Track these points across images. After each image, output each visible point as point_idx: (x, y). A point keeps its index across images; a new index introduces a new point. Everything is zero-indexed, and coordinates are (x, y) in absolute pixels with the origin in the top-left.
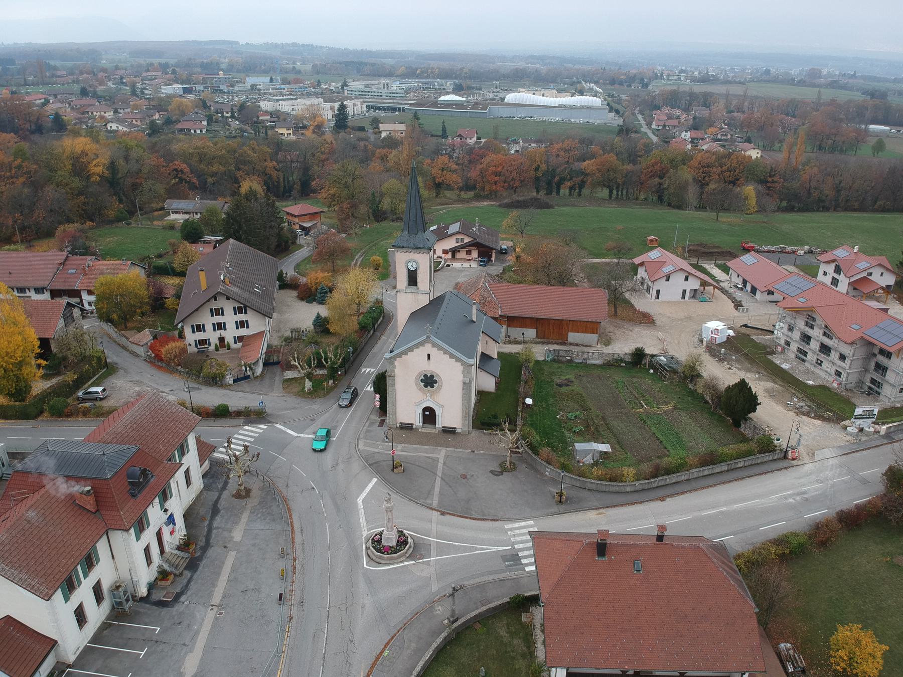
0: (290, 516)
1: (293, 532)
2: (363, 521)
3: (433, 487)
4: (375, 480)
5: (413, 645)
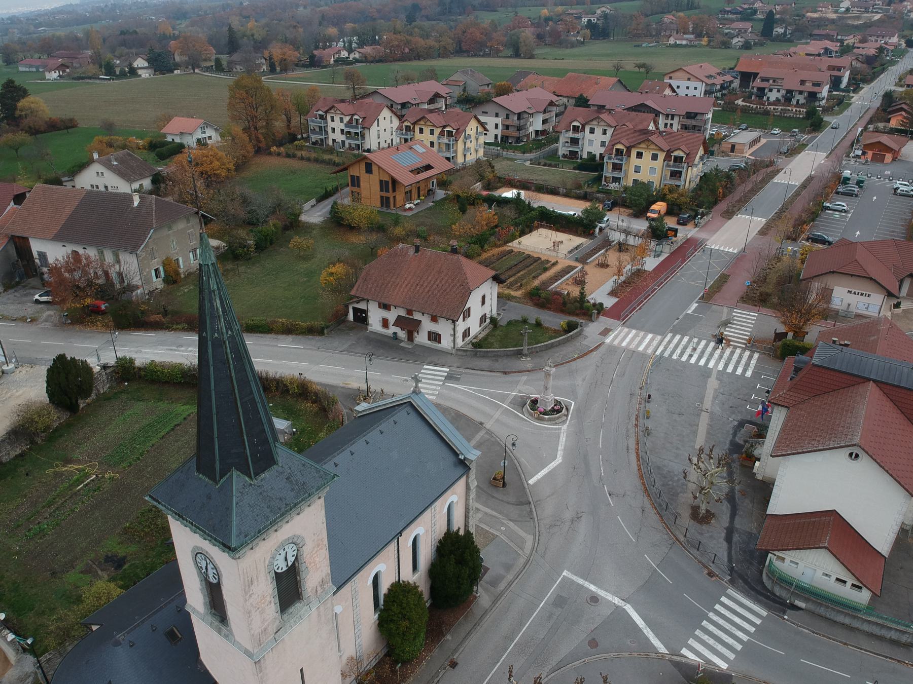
0: (640, 469)
1: (637, 449)
2: (563, 439)
4: (531, 482)
5: (557, 355)
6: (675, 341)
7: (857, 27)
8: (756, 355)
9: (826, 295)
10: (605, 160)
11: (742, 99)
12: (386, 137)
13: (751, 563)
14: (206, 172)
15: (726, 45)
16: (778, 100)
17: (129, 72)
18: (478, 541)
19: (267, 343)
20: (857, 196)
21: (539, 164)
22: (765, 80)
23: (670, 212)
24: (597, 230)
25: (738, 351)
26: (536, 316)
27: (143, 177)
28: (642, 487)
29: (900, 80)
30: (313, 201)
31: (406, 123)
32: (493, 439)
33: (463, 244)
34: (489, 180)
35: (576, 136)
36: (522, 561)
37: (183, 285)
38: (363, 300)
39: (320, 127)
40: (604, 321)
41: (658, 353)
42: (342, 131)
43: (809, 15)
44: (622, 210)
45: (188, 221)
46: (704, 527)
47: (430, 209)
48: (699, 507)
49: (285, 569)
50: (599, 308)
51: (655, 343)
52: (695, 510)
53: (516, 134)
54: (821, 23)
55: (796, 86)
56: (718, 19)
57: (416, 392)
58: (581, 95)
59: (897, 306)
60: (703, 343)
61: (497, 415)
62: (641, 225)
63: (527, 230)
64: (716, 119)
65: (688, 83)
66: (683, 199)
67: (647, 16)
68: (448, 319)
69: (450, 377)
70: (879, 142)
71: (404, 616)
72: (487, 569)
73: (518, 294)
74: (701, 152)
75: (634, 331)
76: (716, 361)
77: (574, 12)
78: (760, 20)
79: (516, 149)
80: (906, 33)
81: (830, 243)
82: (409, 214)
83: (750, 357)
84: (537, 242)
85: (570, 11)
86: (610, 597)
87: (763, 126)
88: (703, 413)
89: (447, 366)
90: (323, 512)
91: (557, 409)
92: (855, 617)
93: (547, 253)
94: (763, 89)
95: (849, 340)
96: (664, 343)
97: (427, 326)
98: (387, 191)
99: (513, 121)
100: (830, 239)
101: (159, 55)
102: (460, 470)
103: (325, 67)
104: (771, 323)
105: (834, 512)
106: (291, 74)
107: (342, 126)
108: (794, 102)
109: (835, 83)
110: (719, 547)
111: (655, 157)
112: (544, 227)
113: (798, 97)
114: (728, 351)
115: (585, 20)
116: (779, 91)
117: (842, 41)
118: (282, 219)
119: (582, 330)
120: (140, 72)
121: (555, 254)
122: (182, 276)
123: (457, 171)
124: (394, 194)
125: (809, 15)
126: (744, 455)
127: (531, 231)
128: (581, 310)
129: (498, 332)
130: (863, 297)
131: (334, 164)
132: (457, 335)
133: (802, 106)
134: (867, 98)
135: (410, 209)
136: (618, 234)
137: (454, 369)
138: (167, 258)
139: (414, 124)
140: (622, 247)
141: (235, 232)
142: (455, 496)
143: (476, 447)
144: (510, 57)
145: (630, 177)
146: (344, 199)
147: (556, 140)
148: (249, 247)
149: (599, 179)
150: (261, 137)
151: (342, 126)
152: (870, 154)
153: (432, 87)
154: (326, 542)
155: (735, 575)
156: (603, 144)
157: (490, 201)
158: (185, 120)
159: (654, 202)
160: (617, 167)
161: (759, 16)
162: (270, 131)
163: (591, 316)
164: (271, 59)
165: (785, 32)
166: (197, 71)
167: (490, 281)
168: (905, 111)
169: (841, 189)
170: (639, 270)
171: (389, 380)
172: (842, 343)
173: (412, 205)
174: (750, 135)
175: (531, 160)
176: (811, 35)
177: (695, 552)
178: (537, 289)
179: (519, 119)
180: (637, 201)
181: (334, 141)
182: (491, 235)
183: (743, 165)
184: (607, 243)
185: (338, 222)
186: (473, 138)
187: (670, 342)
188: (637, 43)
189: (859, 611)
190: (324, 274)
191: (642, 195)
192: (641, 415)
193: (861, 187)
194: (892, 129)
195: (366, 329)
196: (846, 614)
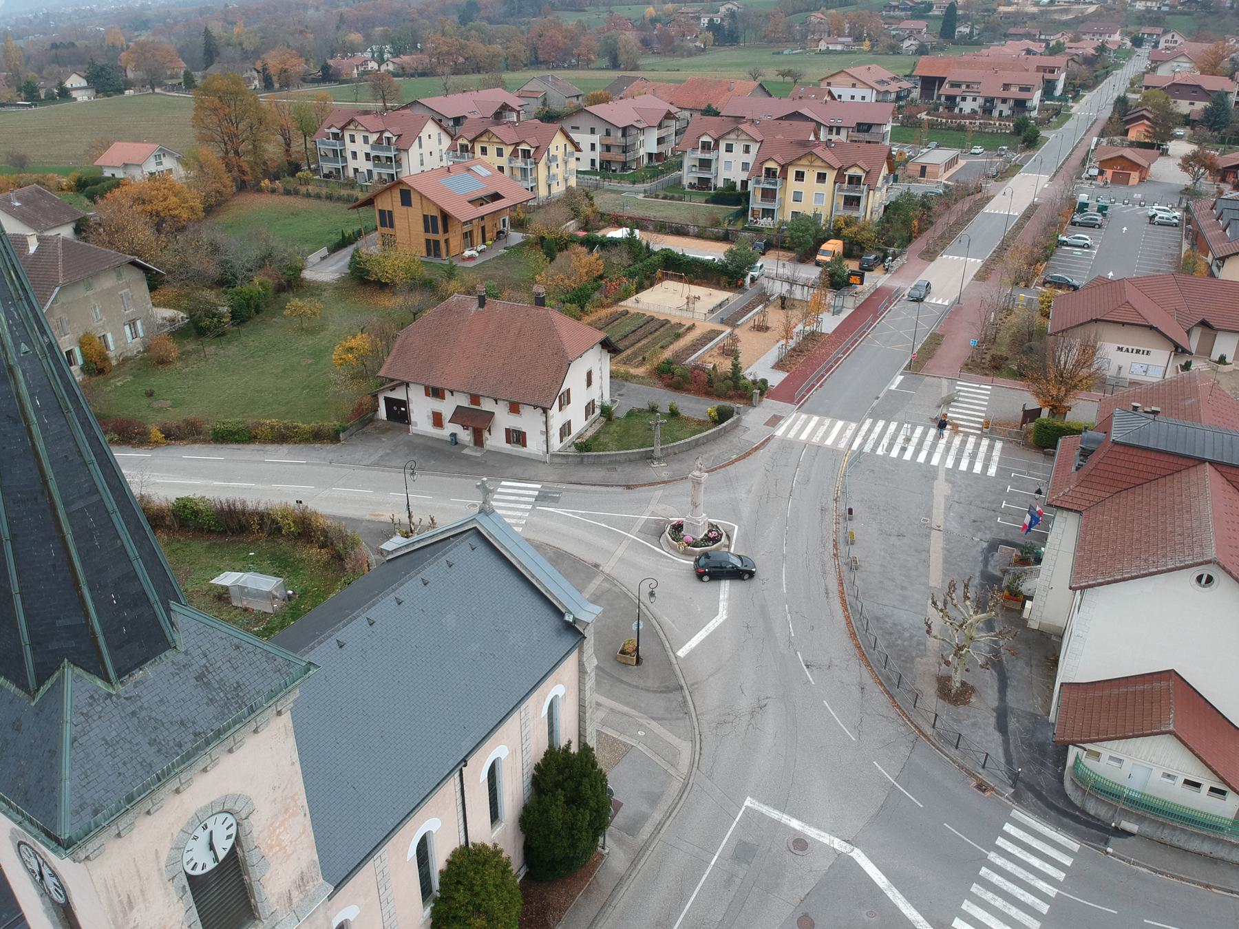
0: (849, 623)
1: (842, 592)
4: (681, 653)
5: (705, 456)
6: (878, 429)
7: (1065, 24)
8: (999, 445)
9: (1089, 351)
10: (750, 188)
11: (929, 107)
12: (432, 163)
13: (1043, 764)
14: (158, 213)
15: (894, 50)
16: (974, 111)
17: (59, 95)
18: (602, 759)
19: (246, 458)
20: (1100, 226)
21: (657, 197)
22: (956, 85)
23: (848, 254)
24: (748, 280)
25: (972, 440)
26: (669, 402)
27: (60, 223)
28: (857, 651)
29: (1132, 84)
30: (324, 251)
32: (617, 590)
35: (707, 156)
36: (676, 786)
37: (114, 377)
39: (335, 151)
40: (769, 406)
41: (855, 447)
42: (367, 155)
43: (1001, 9)
44: (781, 253)
45: (119, 275)
46: (962, 709)
47: (502, 257)
48: (949, 678)
49: (211, 866)
50: (762, 386)
51: (849, 433)
52: (943, 685)
53: (622, 158)
54: (1018, 18)
55: (998, 92)
56: (883, 18)
57: (485, 511)
58: (709, 106)
60: (919, 430)
62: (810, 273)
63: (646, 283)
64: (896, 136)
65: (853, 91)
66: (866, 235)
68: (535, 407)
69: (542, 498)
70: (1122, 157)
71: (478, 908)
72: (619, 805)
74: (885, 171)
75: (816, 418)
76: (942, 455)
77: (690, 10)
78: (936, 17)
79: (622, 178)
80: (1131, 28)
81: (1075, 288)
82: (471, 264)
84: (664, 299)
85: (684, 10)
86: (825, 838)
87: (960, 145)
88: (934, 532)
89: (538, 481)
90: (292, 741)
92: (1218, 841)
93: (679, 313)
94: (954, 98)
97: (504, 419)
98: (435, 231)
100: (1076, 282)
101: (102, 69)
102: (568, 641)
103: (346, 82)
104: (1019, 398)
105: (1171, 674)
106: (294, 91)
107: (367, 149)
108: (996, 114)
109: (1049, 88)
110: (987, 740)
111: (821, 177)
112: (672, 278)
113: (1000, 107)
114: (957, 441)
116: (974, 100)
117: (1047, 42)
118: (271, 261)
119: (739, 420)
120: (74, 94)
121: (690, 315)
122: (114, 363)
123: (539, 207)
125: (1001, 9)
126: (1006, 593)
127: (652, 285)
128: (734, 391)
129: (613, 427)
130: (1140, 355)
132: (551, 432)
134: (1094, 106)
135: (471, 258)
136: (778, 283)
137: (550, 485)
138: (86, 335)
139: (473, 141)
140: (784, 303)
141: (197, 294)
142: (560, 687)
143: (595, 600)
144: (607, 69)
145: (787, 209)
146: (371, 247)
147: (680, 166)
148: (221, 316)
149: (744, 213)
150: (246, 168)
151: (367, 149)
152: (1109, 173)
153: (497, 96)
154: (302, 800)
156: (745, 166)
157: (590, 243)
158: (131, 145)
160: (769, 195)
161: (936, 12)
162: (257, 161)
163: (751, 398)
164: (265, 69)
165: (971, 32)
166: (157, 90)
167: (598, 348)
168: (1148, 119)
169: (1077, 218)
171: (442, 503)
173: (474, 252)
175: (645, 191)
177: (952, 752)
178: (669, 362)
179: (624, 135)
180: (801, 241)
181: (356, 170)
182: (595, 289)
184: (764, 298)
185: (363, 279)
186: (560, 161)
187: (870, 431)
188: (776, 50)
189: (1223, 829)
190: (338, 350)
191: (807, 230)
192: (841, 540)
193: (1104, 215)
196: (1205, 838)
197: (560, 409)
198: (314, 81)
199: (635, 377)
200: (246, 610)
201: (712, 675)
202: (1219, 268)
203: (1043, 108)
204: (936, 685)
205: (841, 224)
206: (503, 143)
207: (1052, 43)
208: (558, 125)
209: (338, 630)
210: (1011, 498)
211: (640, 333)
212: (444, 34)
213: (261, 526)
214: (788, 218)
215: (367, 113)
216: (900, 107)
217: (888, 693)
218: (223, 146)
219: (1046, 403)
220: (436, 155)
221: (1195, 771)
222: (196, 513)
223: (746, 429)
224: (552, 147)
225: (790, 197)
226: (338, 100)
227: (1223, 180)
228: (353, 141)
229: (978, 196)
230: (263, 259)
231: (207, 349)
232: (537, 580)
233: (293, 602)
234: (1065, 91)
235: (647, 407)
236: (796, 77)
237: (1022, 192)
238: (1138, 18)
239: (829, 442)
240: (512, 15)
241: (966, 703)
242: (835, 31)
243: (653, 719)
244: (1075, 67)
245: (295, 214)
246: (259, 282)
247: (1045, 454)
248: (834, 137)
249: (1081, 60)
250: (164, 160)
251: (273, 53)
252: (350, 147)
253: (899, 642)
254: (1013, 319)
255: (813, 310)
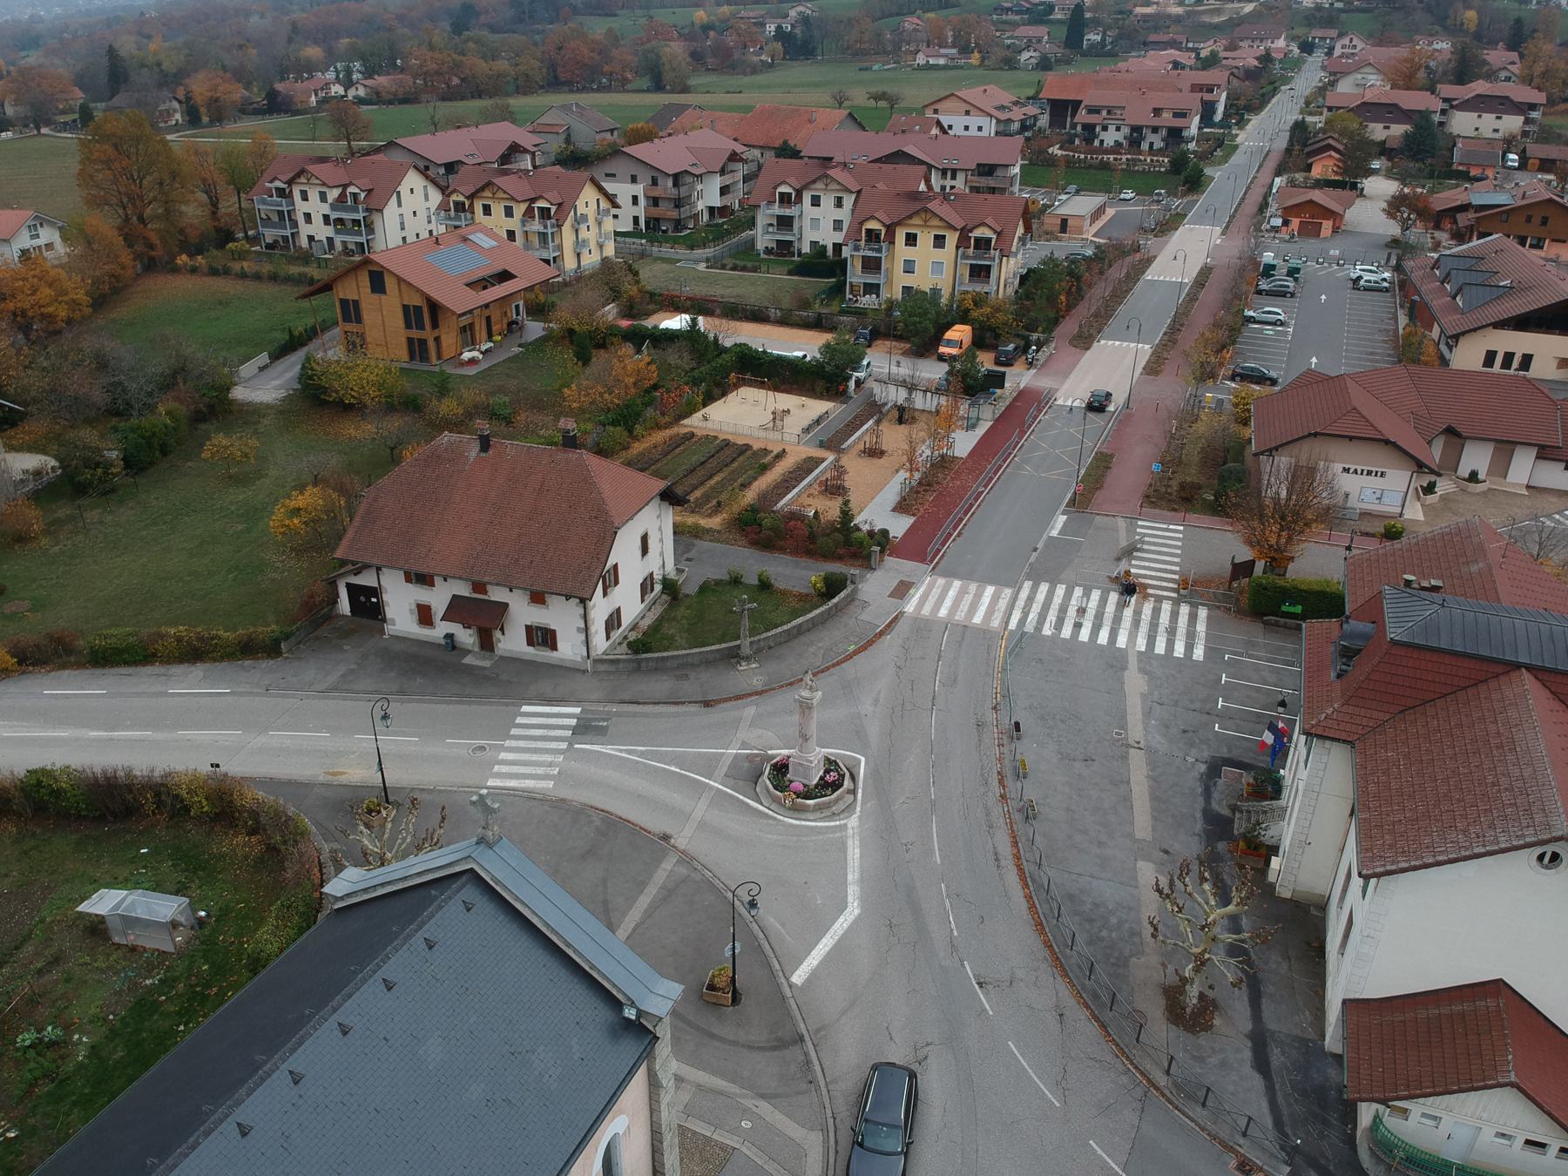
0: (1032, 907)
1: (1017, 857)
2: (854, 852)
3: (649, 913)
4: (798, 978)
5: (812, 649)
6: (1041, 596)
8: (1203, 613)
9: (1303, 477)
11: (1062, 143)
12: (419, 227)
14: (24, 312)
15: (1010, 64)
20: (1293, 295)
21: (723, 267)
22: (1094, 110)
23: (979, 343)
24: (852, 384)
25: (1166, 607)
29: (1307, 103)
30: (263, 358)
31: (454, 197)
32: (698, 877)
33: (589, 426)
34: (631, 299)
35: (787, 212)
38: (366, 567)
39: (280, 213)
40: (893, 569)
41: (1013, 625)
42: (326, 218)
43: (1139, 10)
46: (1203, 1039)
51: (1003, 604)
52: (1173, 996)
53: (674, 214)
54: (1159, 22)
56: (994, 23)
58: (785, 142)
59: (1430, 489)
61: (700, 809)
62: (932, 371)
63: (717, 391)
65: (967, 120)
67: (875, 19)
69: (584, 729)
70: (1311, 202)
73: (715, 522)
74: (1020, 231)
75: (957, 584)
78: (1060, 22)
79: (675, 242)
80: (1299, 31)
82: (471, 371)
83: (1193, 617)
84: (741, 414)
88: (1132, 752)
89: (577, 703)
91: (832, 781)
93: (762, 434)
94: (1093, 127)
95: (1441, 577)
96: (1021, 603)
97: (522, 613)
98: (421, 327)
99: (665, 189)
100: (1273, 374)
102: (630, 1047)
104: (1225, 545)
105: (1498, 987)
106: (230, 127)
108: (1145, 146)
109: (1208, 110)
110: (1245, 1093)
111: (939, 241)
112: (750, 384)
114: (1147, 609)
115: (771, 28)
116: (1118, 129)
117: (1196, 51)
119: (855, 591)
121: (777, 436)
123: (565, 284)
124: (436, 333)
125: (1139, 10)
127: (724, 394)
129: (681, 611)
131: (312, 281)
132: (593, 629)
133: (1160, 152)
134: (1264, 133)
135: (472, 361)
136: (892, 388)
139: (472, 197)
140: (903, 415)
141: (71, 435)
144: (648, 91)
145: (896, 283)
146: (330, 350)
147: (751, 224)
149: (839, 289)
150: (155, 239)
152: (1295, 223)
153: (504, 133)
155: (1298, 1159)
156: (838, 225)
157: (638, 338)
159: (948, 326)
160: (872, 265)
161: (1058, 15)
163: (868, 557)
164: (188, 99)
165: (1103, 40)
167: (657, 501)
169: (1264, 285)
170: (943, 456)
172: (1425, 584)
173: (475, 354)
174: (1095, 201)
175: (708, 260)
176: (1145, 44)
178: (753, 510)
179: (676, 184)
180: (917, 326)
181: (311, 238)
182: (646, 405)
183: (1089, 252)
184: (874, 409)
185: (317, 399)
186: (591, 221)
187: (1030, 599)
190: (279, 513)
192: (1008, 772)
193: (1296, 280)
194: (1318, 181)
195: (382, 632)
197: (605, 594)
198: (259, 112)
199: (709, 531)
200: (133, 949)
201: (844, 1012)
202: (1450, 348)
203: (1202, 138)
204: (1162, 1002)
205: (969, 304)
206: (513, 199)
207: (1204, 54)
208: (587, 174)
209: (239, 1103)
210: (1228, 692)
211: (713, 463)
212: (432, 47)
213: (159, 803)
214: (898, 295)
215: (323, 160)
216: (1027, 139)
217: (1097, 1019)
218: (121, 211)
219: (1262, 554)
220: (422, 215)
221: (1539, 1127)
222: (57, 793)
223: (865, 604)
224: (580, 204)
225: (899, 266)
226: (285, 140)
227: (1437, 227)
228: (305, 198)
229: (1138, 256)
230: (174, 376)
231: (88, 516)
232: (575, 951)
233: (206, 931)
234: (1226, 115)
235: (726, 577)
236: (892, 101)
237: (1188, 252)
238: (1306, 18)
239: (977, 619)
240: (521, 21)
241: (1208, 1028)
242: (935, 40)
243: (763, 1096)
244: (1235, 82)
245: (224, 303)
246: (165, 411)
247: (1265, 623)
248: (949, 183)
249: (1242, 74)
250: (41, 231)
251: (201, 76)
252: (301, 207)
253: (1104, 933)
254: (1200, 428)
255: (943, 423)
